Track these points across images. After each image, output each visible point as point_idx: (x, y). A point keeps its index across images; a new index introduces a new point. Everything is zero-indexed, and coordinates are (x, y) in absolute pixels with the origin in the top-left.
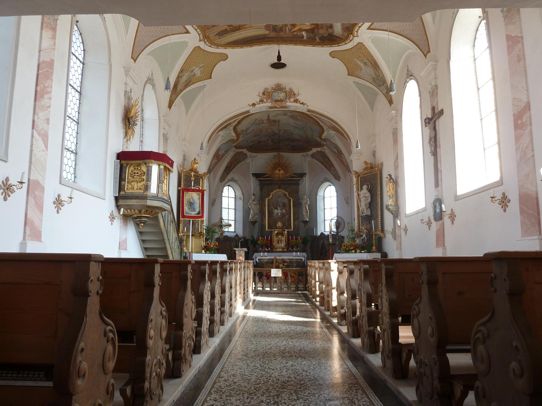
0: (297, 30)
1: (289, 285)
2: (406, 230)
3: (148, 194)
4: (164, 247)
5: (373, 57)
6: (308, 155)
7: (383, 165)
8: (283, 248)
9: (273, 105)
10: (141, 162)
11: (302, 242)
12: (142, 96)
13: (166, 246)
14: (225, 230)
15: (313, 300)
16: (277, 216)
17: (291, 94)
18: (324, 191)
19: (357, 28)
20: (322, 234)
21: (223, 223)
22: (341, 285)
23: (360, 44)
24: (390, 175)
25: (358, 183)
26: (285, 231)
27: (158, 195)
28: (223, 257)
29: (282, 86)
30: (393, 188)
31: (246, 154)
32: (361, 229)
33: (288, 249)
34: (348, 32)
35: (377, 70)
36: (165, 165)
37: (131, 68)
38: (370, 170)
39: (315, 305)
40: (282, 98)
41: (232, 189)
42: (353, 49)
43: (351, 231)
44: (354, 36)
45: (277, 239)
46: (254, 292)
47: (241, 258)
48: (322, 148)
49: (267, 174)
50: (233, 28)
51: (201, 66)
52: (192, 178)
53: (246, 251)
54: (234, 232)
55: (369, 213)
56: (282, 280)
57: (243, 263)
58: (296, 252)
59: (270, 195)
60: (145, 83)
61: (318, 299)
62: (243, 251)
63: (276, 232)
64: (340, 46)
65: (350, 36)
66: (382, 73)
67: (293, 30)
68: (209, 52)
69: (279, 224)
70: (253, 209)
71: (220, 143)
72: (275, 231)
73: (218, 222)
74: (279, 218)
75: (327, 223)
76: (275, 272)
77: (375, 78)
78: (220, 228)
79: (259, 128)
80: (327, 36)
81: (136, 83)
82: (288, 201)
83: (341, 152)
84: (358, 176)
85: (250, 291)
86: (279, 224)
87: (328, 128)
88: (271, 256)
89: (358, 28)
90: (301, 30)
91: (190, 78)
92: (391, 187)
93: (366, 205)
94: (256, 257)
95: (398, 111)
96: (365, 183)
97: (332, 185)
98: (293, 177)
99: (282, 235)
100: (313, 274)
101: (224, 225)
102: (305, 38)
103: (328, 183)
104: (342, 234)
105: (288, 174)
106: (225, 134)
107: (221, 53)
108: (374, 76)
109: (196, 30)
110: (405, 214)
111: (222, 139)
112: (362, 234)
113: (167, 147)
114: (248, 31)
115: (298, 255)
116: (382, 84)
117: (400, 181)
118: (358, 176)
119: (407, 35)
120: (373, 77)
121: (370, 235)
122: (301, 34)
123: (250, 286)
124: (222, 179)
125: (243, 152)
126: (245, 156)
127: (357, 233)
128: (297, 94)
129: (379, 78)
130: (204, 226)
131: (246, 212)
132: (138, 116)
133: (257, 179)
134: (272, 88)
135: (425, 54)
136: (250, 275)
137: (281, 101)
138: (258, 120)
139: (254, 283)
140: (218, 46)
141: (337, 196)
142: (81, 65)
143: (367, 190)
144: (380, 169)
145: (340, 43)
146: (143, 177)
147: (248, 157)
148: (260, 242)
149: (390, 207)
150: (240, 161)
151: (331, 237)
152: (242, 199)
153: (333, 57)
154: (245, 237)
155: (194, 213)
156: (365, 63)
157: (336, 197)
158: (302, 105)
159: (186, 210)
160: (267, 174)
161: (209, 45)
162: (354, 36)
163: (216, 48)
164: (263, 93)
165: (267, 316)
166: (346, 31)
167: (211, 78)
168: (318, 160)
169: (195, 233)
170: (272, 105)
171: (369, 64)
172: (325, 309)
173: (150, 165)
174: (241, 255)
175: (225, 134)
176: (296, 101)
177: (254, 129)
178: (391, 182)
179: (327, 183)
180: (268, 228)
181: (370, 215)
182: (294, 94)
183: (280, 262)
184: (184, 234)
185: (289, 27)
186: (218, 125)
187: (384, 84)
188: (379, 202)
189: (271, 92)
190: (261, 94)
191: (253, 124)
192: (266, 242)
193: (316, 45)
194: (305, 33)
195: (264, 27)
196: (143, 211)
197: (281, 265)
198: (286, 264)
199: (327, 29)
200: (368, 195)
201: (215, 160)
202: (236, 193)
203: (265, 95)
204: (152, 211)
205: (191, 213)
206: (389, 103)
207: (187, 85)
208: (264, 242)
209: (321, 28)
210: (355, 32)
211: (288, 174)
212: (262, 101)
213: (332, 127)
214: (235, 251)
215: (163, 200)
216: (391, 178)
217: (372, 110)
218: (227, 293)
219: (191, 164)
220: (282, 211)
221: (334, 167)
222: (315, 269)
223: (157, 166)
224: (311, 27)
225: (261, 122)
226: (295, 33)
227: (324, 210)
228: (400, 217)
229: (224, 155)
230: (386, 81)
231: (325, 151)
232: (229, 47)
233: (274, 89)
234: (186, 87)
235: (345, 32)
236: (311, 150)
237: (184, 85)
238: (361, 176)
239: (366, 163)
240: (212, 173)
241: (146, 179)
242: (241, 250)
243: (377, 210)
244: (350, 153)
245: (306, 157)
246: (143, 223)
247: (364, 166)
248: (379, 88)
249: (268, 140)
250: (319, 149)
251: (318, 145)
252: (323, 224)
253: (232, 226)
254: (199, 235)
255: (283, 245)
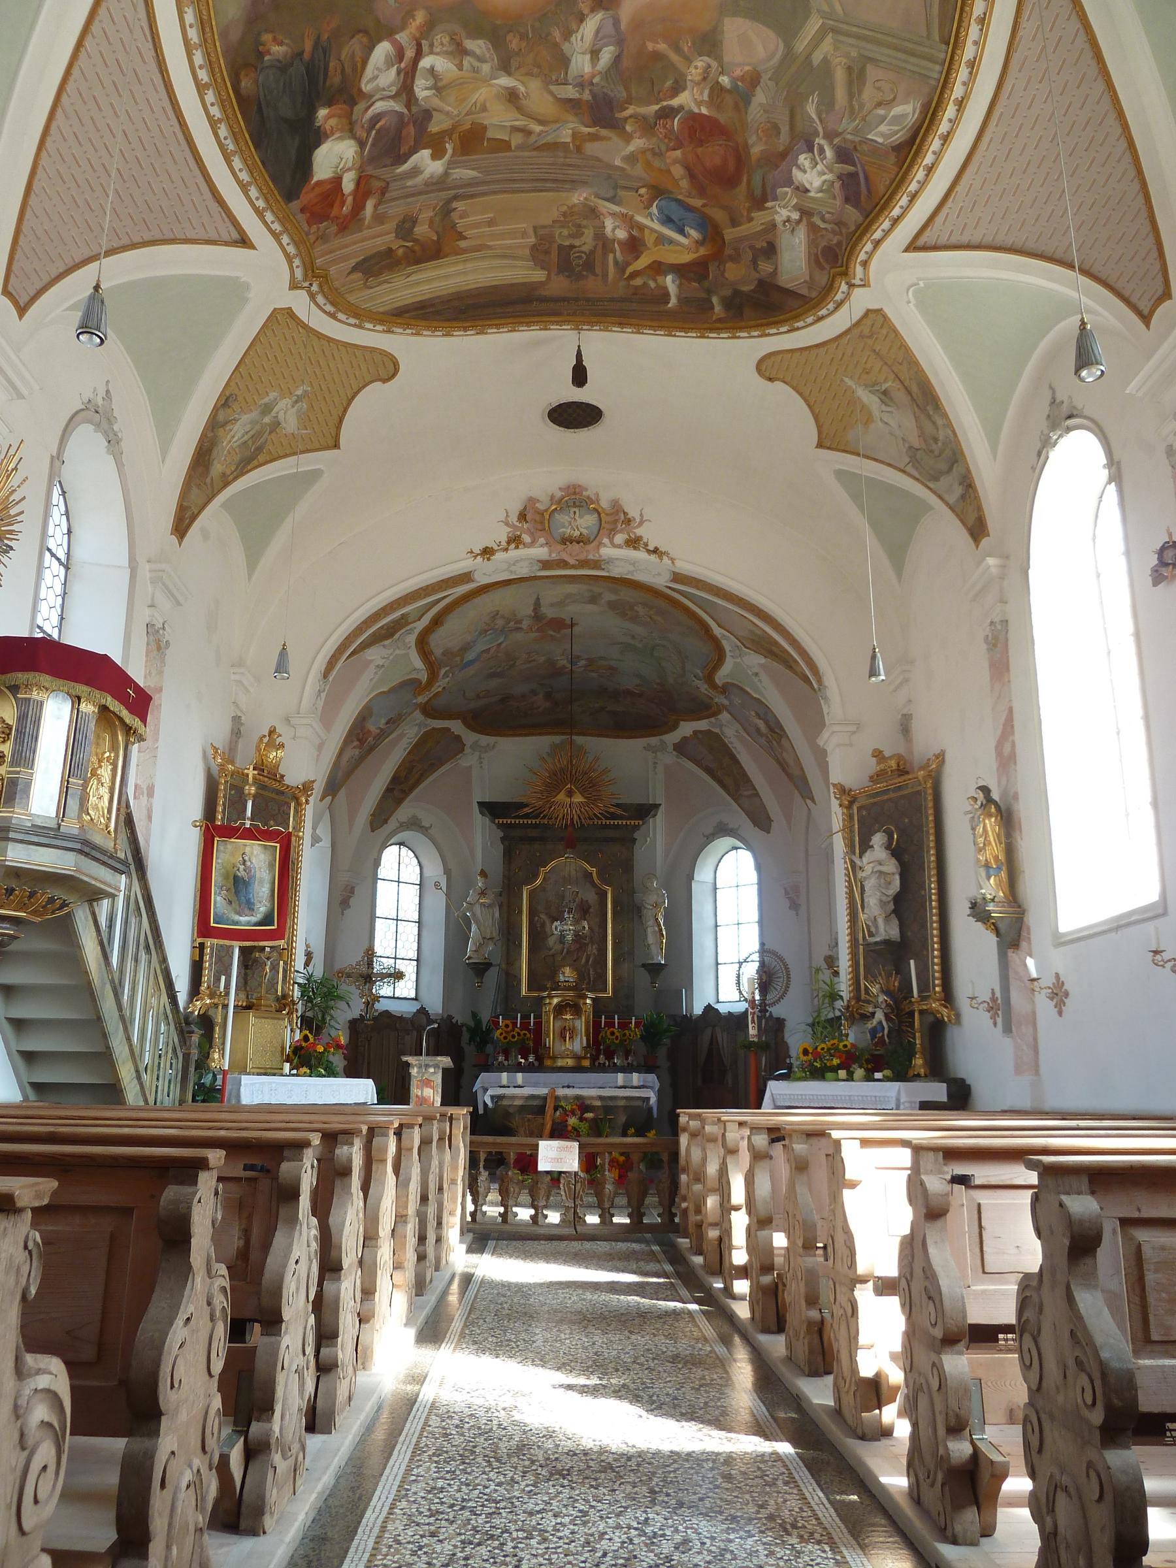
0: (646, 268)
2: (1059, 994)
3: (17, 816)
4: (99, 1048)
8: (578, 1058)
9: (554, 555)
11: (642, 1037)
12: (52, 457)
13: (108, 1048)
14: (382, 992)
15: (711, 1287)
16: (558, 947)
20: (709, 1008)
21: (377, 968)
22: (944, 1290)
23: (871, 316)
24: (985, 790)
26: (586, 997)
27: (59, 825)
28: (362, 1090)
30: (998, 835)
31: (458, 738)
32: (863, 992)
33: (594, 1059)
34: (831, 268)
36: (103, 702)
38: (896, 781)
39: (730, 1318)
40: (585, 532)
41: (411, 854)
42: (845, 340)
43: (827, 1001)
44: (854, 285)
45: (559, 1024)
46: (469, 1231)
47: (428, 1092)
48: (713, 720)
49: (527, 805)
50: (417, 248)
51: (299, 392)
52: (247, 787)
53: (447, 1066)
54: (412, 999)
55: (894, 933)
56: (579, 1186)
58: (627, 1069)
59: (536, 876)
61: (742, 1286)
62: (436, 1066)
63: (555, 1001)
64: (798, 329)
65: (836, 285)
66: (949, 425)
67: (630, 270)
68: (330, 340)
69: (567, 974)
70: (477, 922)
71: (370, 693)
72: (550, 997)
73: (358, 964)
74: (568, 952)
75: (727, 976)
76: (553, 1154)
77: (917, 450)
78: (365, 983)
79: (504, 645)
80: (753, 291)
82: (596, 897)
84: (851, 803)
85: (453, 1233)
86: (567, 974)
87: (739, 644)
88: (535, 1085)
90: (658, 268)
92: (990, 833)
93: (883, 904)
94: (486, 1086)
95: (1007, 557)
96: (877, 827)
97: (741, 845)
98: (614, 816)
99: (577, 1010)
101: (377, 975)
102: (673, 301)
103: (729, 841)
105: (598, 806)
106: (388, 658)
107: (373, 350)
109: (276, 236)
110: (1056, 934)
112: (871, 1010)
113: (160, 673)
114: (470, 265)
115: (635, 1083)
116: (943, 466)
117: (1024, 810)
118: (851, 803)
119: (1065, 253)
120: (911, 447)
121: (900, 1012)
122: (658, 287)
123: (452, 1213)
124: (379, 818)
125: (448, 729)
126: (456, 746)
128: (638, 520)
129: (934, 447)
130: (298, 972)
131: (456, 932)
132: (19, 518)
134: (552, 497)
136: (455, 1168)
137: (581, 540)
138: (503, 617)
139: (469, 1198)
140: (361, 316)
141: (760, 883)
143: (887, 848)
144: (933, 773)
145: (797, 318)
147: (467, 750)
148: (501, 1034)
149: (990, 907)
150: (441, 762)
151: (753, 1018)
152: (444, 889)
153: (770, 380)
154: (450, 1017)
155: (247, 918)
156: (885, 393)
158: (653, 557)
159: (218, 905)
160: (527, 805)
161: (329, 308)
163: (355, 326)
164: (520, 514)
165: (521, 1403)
166: (824, 264)
167: (336, 446)
168: (697, 762)
171: (900, 396)
172: (789, 1358)
173: (35, 695)
174: (427, 1083)
175: (388, 658)
176: (634, 543)
178: (990, 815)
179: (727, 842)
180: (530, 989)
181: (899, 940)
182: (628, 521)
183: (569, 1108)
185: (618, 254)
188: (931, 894)
189: (546, 511)
190: (514, 519)
191: (486, 631)
192: (519, 1034)
193: (712, 330)
194: (673, 281)
195: (527, 252)
197: (572, 1121)
198: (590, 1115)
199: (754, 262)
200: (891, 866)
202: (425, 870)
203: (527, 522)
204: (32, 895)
205: (237, 918)
207: (248, 461)
208: (513, 1037)
210: (858, 265)
211: (598, 806)
212: (515, 541)
214: (408, 1065)
215: (87, 849)
216: (989, 800)
217: (900, 581)
218: (291, 1329)
219: (258, 749)
220: (579, 928)
221: (753, 785)
224: (695, 256)
225: (512, 624)
226: (638, 282)
227: (714, 931)
228: (1029, 943)
229: (382, 735)
230: (962, 453)
231: (721, 731)
232: (407, 326)
233: (560, 501)
234: (246, 464)
235: (822, 268)
236: (675, 727)
237: (237, 458)
238: (862, 801)
239: (878, 754)
240: (342, 793)
241: (13, 756)
242: (431, 1064)
243: (923, 925)
244: (815, 723)
247: (872, 766)
249: (534, 693)
250: (702, 725)
251: (702, 709)
253: (406, 978)
255: (577, 1045)
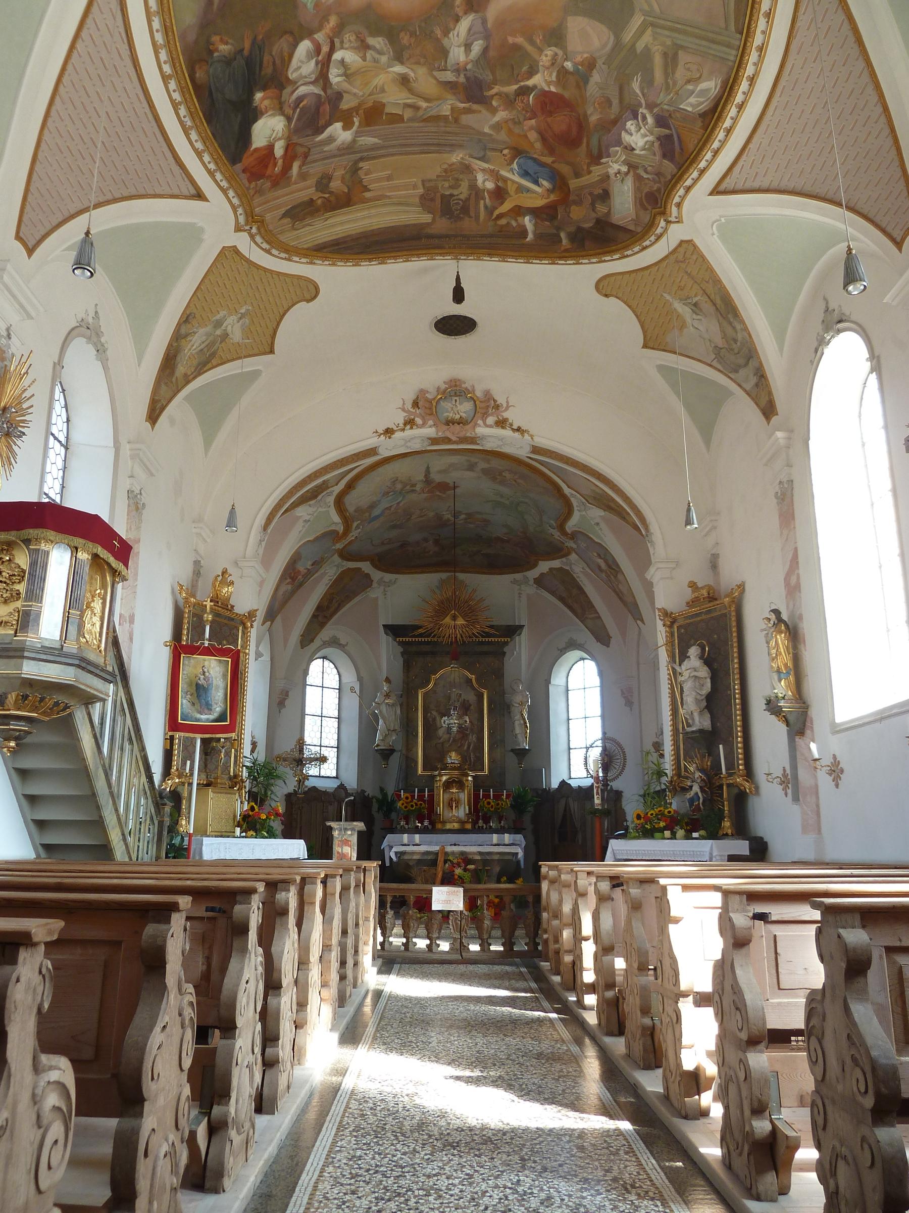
1: (485, 937)
2: (836, 771)
3: (30, 639)
5: (720, 281)
6: (526, 577)
7: (744, 588)
8: (462, 822)
9: (440, 434)
10: (11, 536)
11: (512, 806)
13: (101, 817)
14: (311, 773)
16: (446, 736)
17: (488, 406)
18: (567, 672)
19: (679, 194)
20: (563, 783)
21: (306, 754)
23: (684, 245)
24: (777, 612)
25: (672, 643)
26: (468, 775)
27: (62, 646)
28: (296, 848)
29: (463, 386)
31: (368, 576)
32: (683, 770)
33: (475, 823)
35: (730, 323)
36: (95, 551)
37: (9, 260)
38: (707, 606)
40: (464, 415)
41: (332, 665)
43: (655, 777)
44: (670, 222)
46: (379, 957)
47: (347, 850)
48: (564, 559)
51: (243, 311)
52: (206, 615)
53: (359, 829)
54: (334, 777)
56: (463, 922)
57: (338, 878)
59: (428, 682)
60: (69, 333)
61: (591, 1000)
62: (353, 829)
63: (444, 778)
66: (746, 329)
67: (497, 212)
69: (453, 758)
70: (384, 718)
72: (441, 775)
73: (292, 750)
74: (454, 740)
76: (444, 897)
77: (721, 349)
78: (298, 766)
79: (402, 503)
81: (30, 317)
83: (618, 565)
84: (673, 623)
85: (367, 959)
86: (453, 758)
87: (584, 500)
89: (681, 192)
90: (518, 211)
91: (213, 343)
92: (781, 646)
93: (697, 701)
95: (792, 431)
98: (488, 635)
99: (461, 785)
100: (567, 908)
101: (307, 759)
102: (530, 237)
103: (578, 653)
104: (615, 785)
105: (475, 628)
106: (313, 515)
107: (299, 277)
108: (720, 343)
110: (833, 724)
111: (304, 529)
112: (689, 784)
113: (138, 528)
114: (373, 211)
115: (507, 842)
116: (741, 361)
117: (807, 628)
118: (673, 623)
120: (716, 347)
121: (712, 785)
122: (519, 225)
123: (366, 943)
124: (307, 638)
125: (360, 569)
126: (366, 582)
127: (672, 781)
128: (505, 405)
129: (734, 346)
130: (245, 757)
131: (368, 725)
132: (30, 411)
133: (395, 640)
135: (898, 239)
137: (461, 422)
138: (401, 482)
139: (379, 931)
140: (290, 251)
142: (63, 450)
143: (700, 658)
144: (736, 600)
145: (626, 248)
146: (17, 587)
147: (375, 585)
148: (403, 804)
149: (782, 704)
150: (356, 594)
151: (597, 790)
152: (358, 692)
153: (606, 296)
154: (363, 791)
156: (695, 305)
157: (599, 689)
158: (517, 435)
161: (265, 246)
162: (670, 222)
163: (285, 259)
167: (272, 352)
168: (553, 593)
169: (216, 778)
170: (437, 434)
171: (707, 306)
173: (43, 546)
174: (346, 842)
175: (313, 515)
176: (502, 423)
177: (391, 506)
178: (781, 632)
179: (577, 654)
180: (424, 769)
181: (710, 729)
182: (497, 407)
183: (455, 861)
184: (183, 780)
185: (487, 200)
186: (293, 485)
187: (749, 360)
188: (735, 694)
189: (434, 399)
190: (409, 406)
192: (416, 804)
193: (560, 258)
194: (530, 221)
195: (417, 200)
196: (12, 698)
198: (472, 867)
199: (593, 204)
200: (704, 672)
201: (288, 584)
202: (343, 678)
203: (419, 408)
204: (42, 700)
205: (198, 716)
206: (764, 414)
207: (204, 364)
209: (575, 203)
210: (673, 206)
211: (475, 628)
213: (595, 498)
214: (331, 828)
216: (780, 620)
220: (461, 722)
221: (596, 610)
222: (574, 895)
223: (68, 555)
225: (408, 487)
226: (503, 222)
228: (812, 731)
229: (309, 573)
233: (444, 392)
234: (201, 369)
235: (646, 209)
236: (535, 565)
238: (681, 622)
239: (693, 585)
240: (279, 619)
241: (26, 593)
243: (730, 718)
244: (644, 561)
245: (522, 586)
246: (16, 739)
247: (689, 594)
248: (733, 377)
249: (426, 540)
250: (556, 564)
251: (557, 551)
252: (566, 758)
253: (329, 762)
254: (228, 783)
255: (462, 812)
